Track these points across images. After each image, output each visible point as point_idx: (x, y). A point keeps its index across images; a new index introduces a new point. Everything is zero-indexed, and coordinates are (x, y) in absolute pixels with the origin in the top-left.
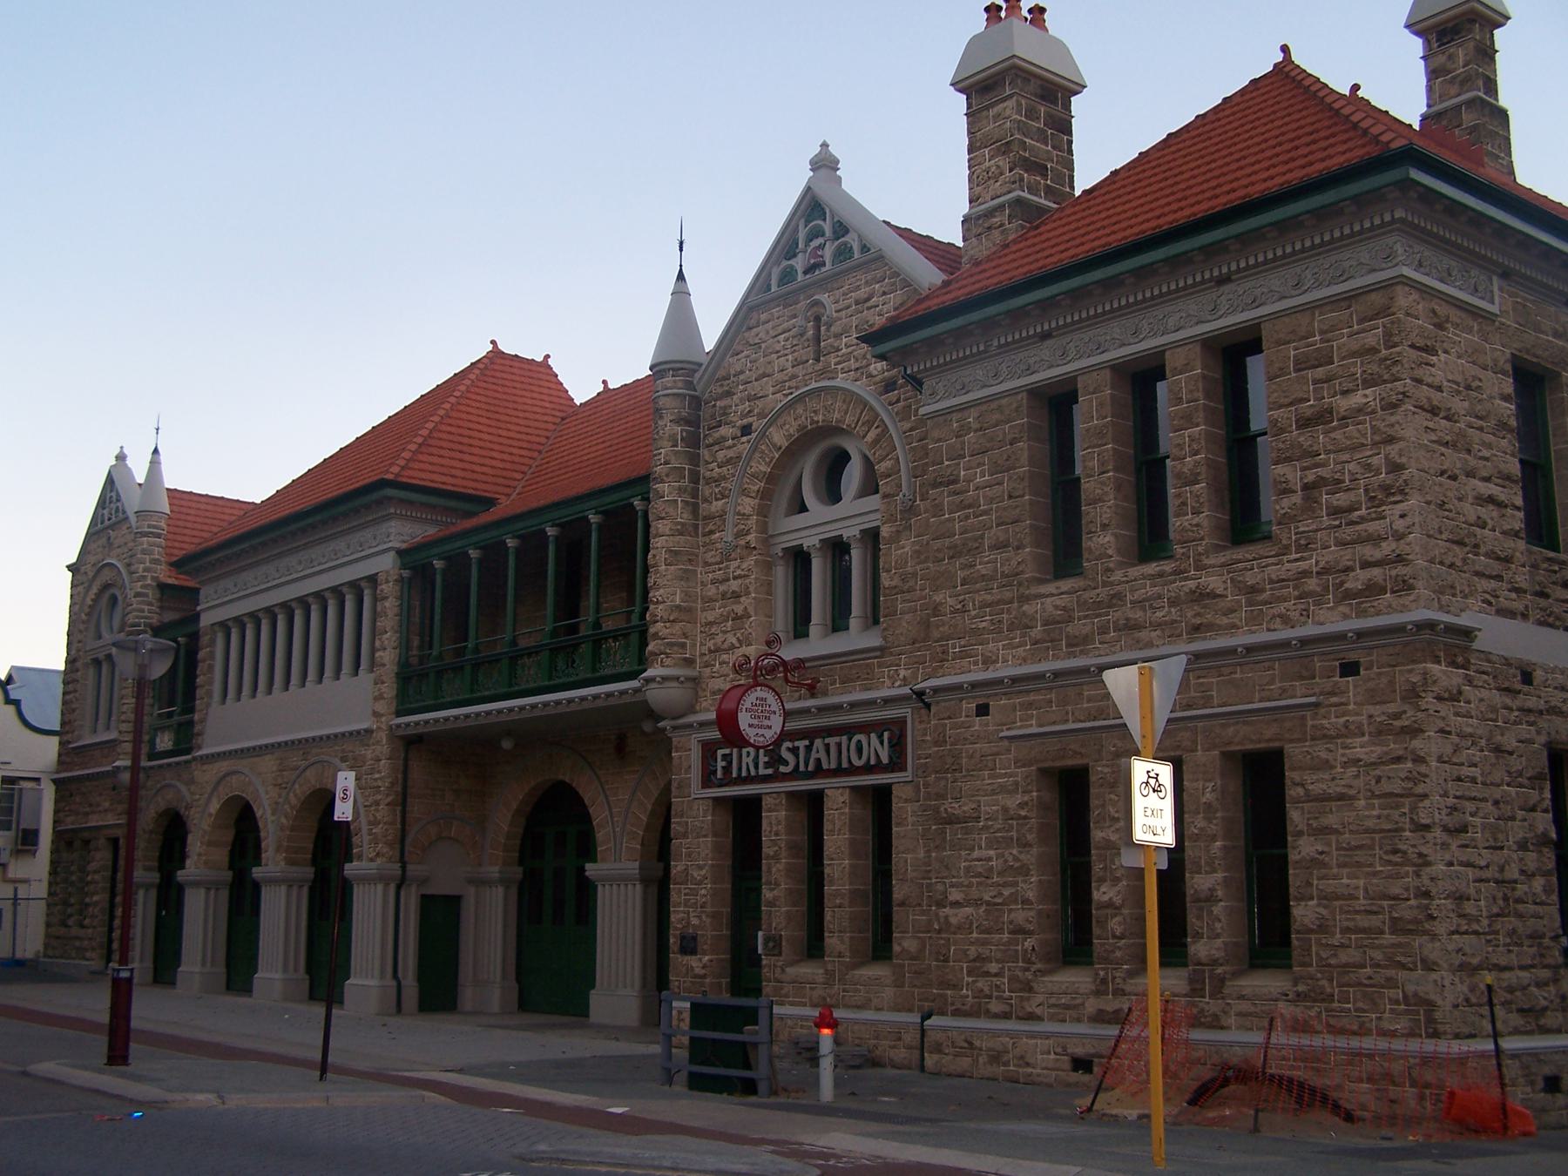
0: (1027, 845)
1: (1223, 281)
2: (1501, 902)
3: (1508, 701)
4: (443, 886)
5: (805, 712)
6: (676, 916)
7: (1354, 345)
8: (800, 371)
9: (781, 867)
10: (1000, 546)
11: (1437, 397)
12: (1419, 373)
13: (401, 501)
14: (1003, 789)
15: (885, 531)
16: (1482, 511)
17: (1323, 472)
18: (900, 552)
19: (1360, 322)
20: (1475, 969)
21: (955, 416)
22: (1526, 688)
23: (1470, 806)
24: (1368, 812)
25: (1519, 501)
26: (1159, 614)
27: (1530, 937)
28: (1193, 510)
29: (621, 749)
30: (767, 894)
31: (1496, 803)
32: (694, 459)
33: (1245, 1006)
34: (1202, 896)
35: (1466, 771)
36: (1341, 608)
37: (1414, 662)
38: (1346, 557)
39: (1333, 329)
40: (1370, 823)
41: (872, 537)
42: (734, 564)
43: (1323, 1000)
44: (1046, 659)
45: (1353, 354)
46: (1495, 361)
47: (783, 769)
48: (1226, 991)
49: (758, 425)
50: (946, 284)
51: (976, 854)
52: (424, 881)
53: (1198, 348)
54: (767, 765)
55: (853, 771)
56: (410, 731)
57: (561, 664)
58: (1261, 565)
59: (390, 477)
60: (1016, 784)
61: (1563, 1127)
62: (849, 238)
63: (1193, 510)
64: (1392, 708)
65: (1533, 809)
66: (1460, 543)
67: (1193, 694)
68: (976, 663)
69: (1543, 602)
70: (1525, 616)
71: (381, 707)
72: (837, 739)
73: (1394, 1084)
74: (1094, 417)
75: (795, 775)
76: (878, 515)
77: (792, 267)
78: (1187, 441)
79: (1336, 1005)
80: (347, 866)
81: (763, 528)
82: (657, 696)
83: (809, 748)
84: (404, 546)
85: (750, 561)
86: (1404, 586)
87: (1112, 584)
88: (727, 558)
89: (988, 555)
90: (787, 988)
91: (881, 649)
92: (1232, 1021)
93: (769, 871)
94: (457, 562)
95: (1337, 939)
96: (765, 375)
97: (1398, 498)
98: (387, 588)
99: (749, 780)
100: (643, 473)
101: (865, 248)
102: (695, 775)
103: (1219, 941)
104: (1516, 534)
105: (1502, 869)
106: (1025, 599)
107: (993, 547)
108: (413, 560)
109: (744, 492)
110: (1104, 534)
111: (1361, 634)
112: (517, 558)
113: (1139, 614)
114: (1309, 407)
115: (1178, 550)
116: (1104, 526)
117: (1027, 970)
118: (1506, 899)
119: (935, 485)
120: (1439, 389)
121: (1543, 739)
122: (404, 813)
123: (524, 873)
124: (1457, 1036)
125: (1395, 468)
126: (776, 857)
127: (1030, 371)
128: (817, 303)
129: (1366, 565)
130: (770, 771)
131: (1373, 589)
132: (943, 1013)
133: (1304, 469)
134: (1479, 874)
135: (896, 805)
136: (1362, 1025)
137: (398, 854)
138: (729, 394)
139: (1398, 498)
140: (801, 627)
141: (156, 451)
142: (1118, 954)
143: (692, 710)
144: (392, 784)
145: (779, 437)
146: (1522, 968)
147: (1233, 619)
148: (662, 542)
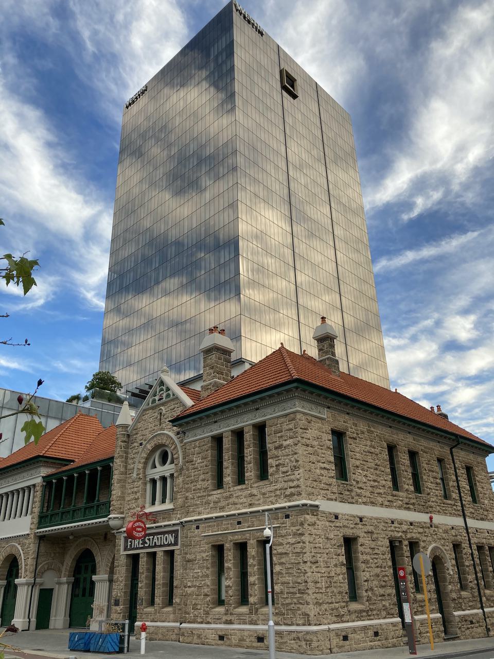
0: (208, 568)
1: (257, 409)
2: (329, 583)
3: (331, 524)
4: (47, 586)
5: (152, 528)
7: (287, 428)
8: (156, 428)
9: (144, 576)
10: (203, 480)
11: (308, 442)
12: (303, 435)
13: (45, 462)
14: (202, 551)
15: (175, 475)
16: (322, 472)
17: (280, 461)
19: (289, 421)
20: (320, 604)
21: (193, 443)
22: (336, 520)
23: (319, 555)
24: (292, 558)
25: (334, 468)
26: (242, 500)
27: (338, 593)
28: (251, 472)
29: (105, 538)
30: (140, 585)
31: (327, 554)
32: (127, 453)
34: (252, 583)
35: (317, 545)
36: (285, 499)
37: (302, 515)
38: (286, 485)
39: (282, 423)
40: (293, 561)
41: (172, 475)
42: (136, 483)
43: (282, 615)
44: (214, 513)
45: (287, 430)
46: (326, 430)
47: (146, 545)
48: (258, 613)
49: (144, 443)
50: (193, 406)
51: (195, 571)
52: (41, 584)
53: (251, 427)
54: (142, 544)
55: (164, 545)
56: (41, 534)
57: (64, 517)
58: (266, 487)
59: (42, 454)
60: (206, 549)
61: (492, 650)
63: (251, 472)
64: (297, 528)
65: (339, 555)
66: (316, 481)
67: (250, 523)
68: (196, 514)
69: (341, 496)
70: (336, 500)
71: (33, 526)
72: (160, 536)
73: (300, 640)
75: (149, 547)
76: (173, 470)
77: (169, 393)
78: (250, 453)
80: (16, 580)
81: (144, 473)
82: (111, 523)
83: (153, 539)
84: (44, 475)
86: (299, 494)
87: (230, 491)
88: (134, 482)
90: (144, 616)
91: (173, 509)
92: (260, 622)
93: (141, 577)
94: (60, 481)
96: (146, 429)
98: (38, 488)
99: (137, 548)
100: (111, 456)
101: (174, 395)
102: (122, 548)
103: (256, 597)
104: (333, 477)
105: (329, 573)
106: (209, 495)
107: (201, 480)
108: (47, 479)
109: (139, 462)
111: (289, 507)
112: (101, 473)
113: (236, 500)
114: (277, 444)
115: (246, 482)
116: (229, 475)
117: (208, 607)
118: (330, 582)
119: (188, 462)
120: (309, 439)
121: (342, 535)
122: (37, 562)
123: (75, 580)
124: (315, 625)
125: (297, 461)
126: (143, 573)
127: (211, 431)
128: (161, 409)
130: (142, 546)
131: (292, 495)
132: (185, 623)
133: (276, 460)
134: (322, 575)
136: (292, 622)
137: (33, 575)
138: (137, 434)
140: (153, 503)
142: (231, 601)
144: (34, 551)
145: (149, 447)
146: (336, 603)
148: (116, 477)
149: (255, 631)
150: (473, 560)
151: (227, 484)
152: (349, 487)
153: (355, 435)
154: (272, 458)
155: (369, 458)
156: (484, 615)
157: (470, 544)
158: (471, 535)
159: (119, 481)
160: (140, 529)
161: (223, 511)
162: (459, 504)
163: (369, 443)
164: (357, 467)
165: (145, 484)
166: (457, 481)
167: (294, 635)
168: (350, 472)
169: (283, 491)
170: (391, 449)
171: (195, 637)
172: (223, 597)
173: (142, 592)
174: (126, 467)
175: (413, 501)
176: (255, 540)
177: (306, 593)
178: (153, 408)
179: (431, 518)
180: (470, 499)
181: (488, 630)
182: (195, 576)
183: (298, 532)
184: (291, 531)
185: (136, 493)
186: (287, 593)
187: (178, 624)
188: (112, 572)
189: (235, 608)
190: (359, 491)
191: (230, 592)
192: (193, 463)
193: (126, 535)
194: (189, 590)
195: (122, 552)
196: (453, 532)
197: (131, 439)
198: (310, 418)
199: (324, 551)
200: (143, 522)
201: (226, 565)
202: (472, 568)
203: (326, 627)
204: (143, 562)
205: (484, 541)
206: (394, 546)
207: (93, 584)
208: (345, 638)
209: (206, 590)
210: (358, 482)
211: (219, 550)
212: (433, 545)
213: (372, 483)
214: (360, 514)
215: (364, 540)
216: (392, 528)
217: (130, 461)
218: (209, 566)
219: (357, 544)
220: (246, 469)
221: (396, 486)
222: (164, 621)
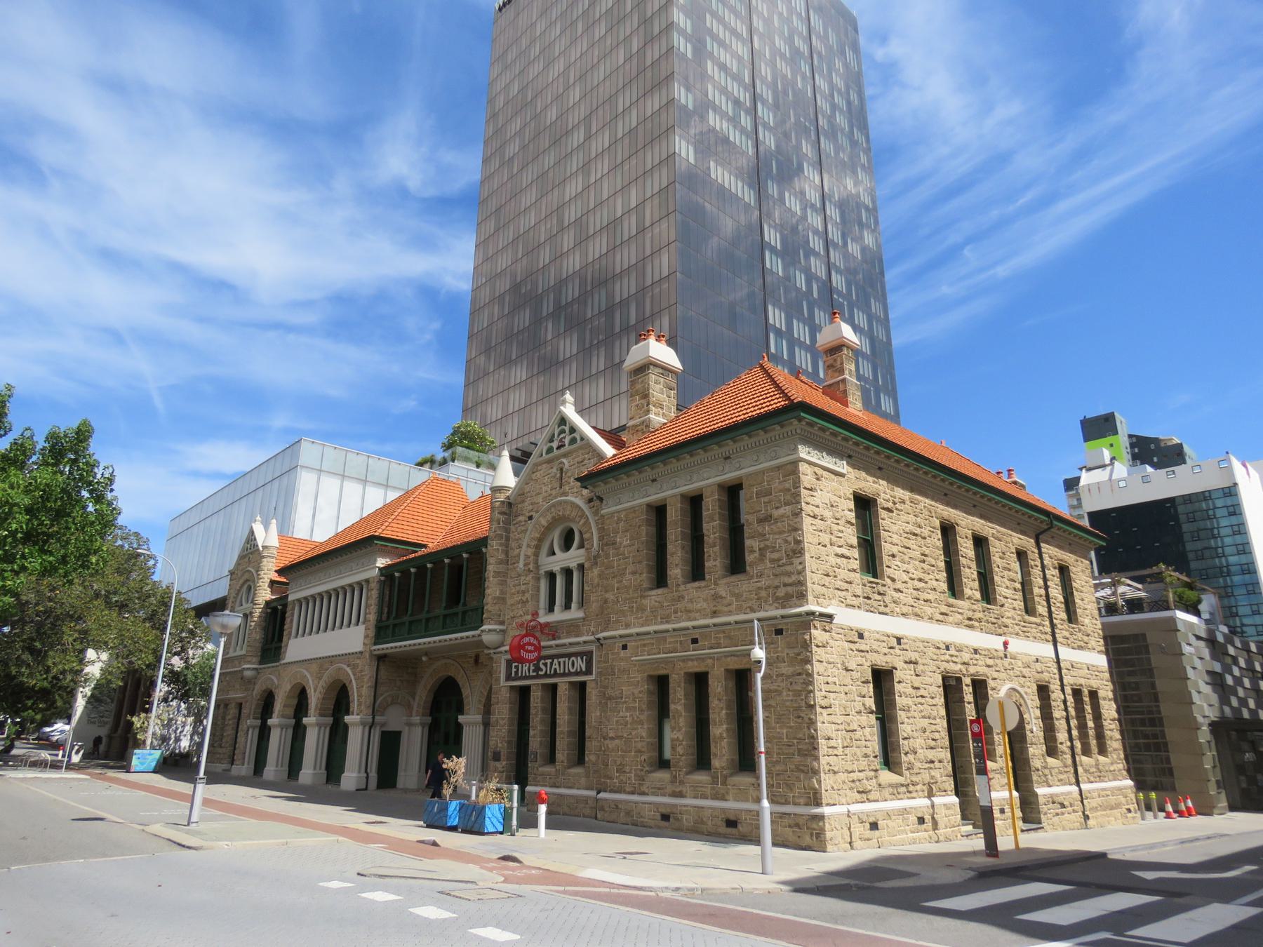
4: (392, 727)
6: (492, 743)
7: (781, 487)
8: (554, 492)
11: (817, 511)
18: (593, 574)
25: (857, 556)
28: (715, 559)
29: (477, 660)
30: (532, 732)
32: (507, 531)
38: (776, 582)
41: (581, 567)
49: (536, 516)
52: (383, 725)
55: (570, 674)
58: (743, 584)
63: (715, 559)
64: (796, 651)
66: (827, 575)
74: (712, 509)
75: (546, 676)
78: (713, 529)
82: (486, 638)
85: (530, 577)
89: (628, 576)
90: (539, 778)
94: (405, 573)
101: (582, 439)
102: (503, 676)
104: (854, 571)
110: (677, 567)
115: (707, 577)
119: (607, 545)
129: (785, 585)
131: (788, 597)
135: (588, 690)
140: (551, 609)
143: (502, 645)
145: (544, 522)
147: (730, 608)
148: (491, 568)
149: (723, 810)
150: (1066, 710)
152: (881, 589)
153: (890, 505)
155: (912, 543)
156: (1081, 795)
157: (1062, 686)
158: (1064, 671)
159: (497, 574)
160: (531, 648)
161: (668, 622)
162: (1047, 623)
163: (911, 518)
164: (893, 556)
165: (538, 579)
166: (1046, 587)
170: (948, 530)
172: (667, 754)
173: (536, 740)
174: (507, 553)
175: (978, 615)
178: (549, 461)
179: (1006, 644)
180: (1064, 616)
181: (1086, 818)
185: (524, 592)
187: (593, 793)
188: (487, 711)
189: (688, 773)
191: (680, 750)
193: (509, 657)
194: (612, 744)
195: (503, 683)
196: (1038, 666)
197: (514, 509)
198: (820, 472)
199: (842, 689)
200: (535, 637)
201: (672, 707)
202: (1063, 722)
203: (843, 809)
204: (536, 699)
205: (1082, 681)
206: (951, 686)
207: (459, 727)
208: (874, 826)
209: (639, 745)
210: (893, 580)
211: (662, 683)
212: (1008, 686)
213: (916, 583)
214: (899, 633)
216: (947, 657)
217: (513, 544)
218: (644, 707)
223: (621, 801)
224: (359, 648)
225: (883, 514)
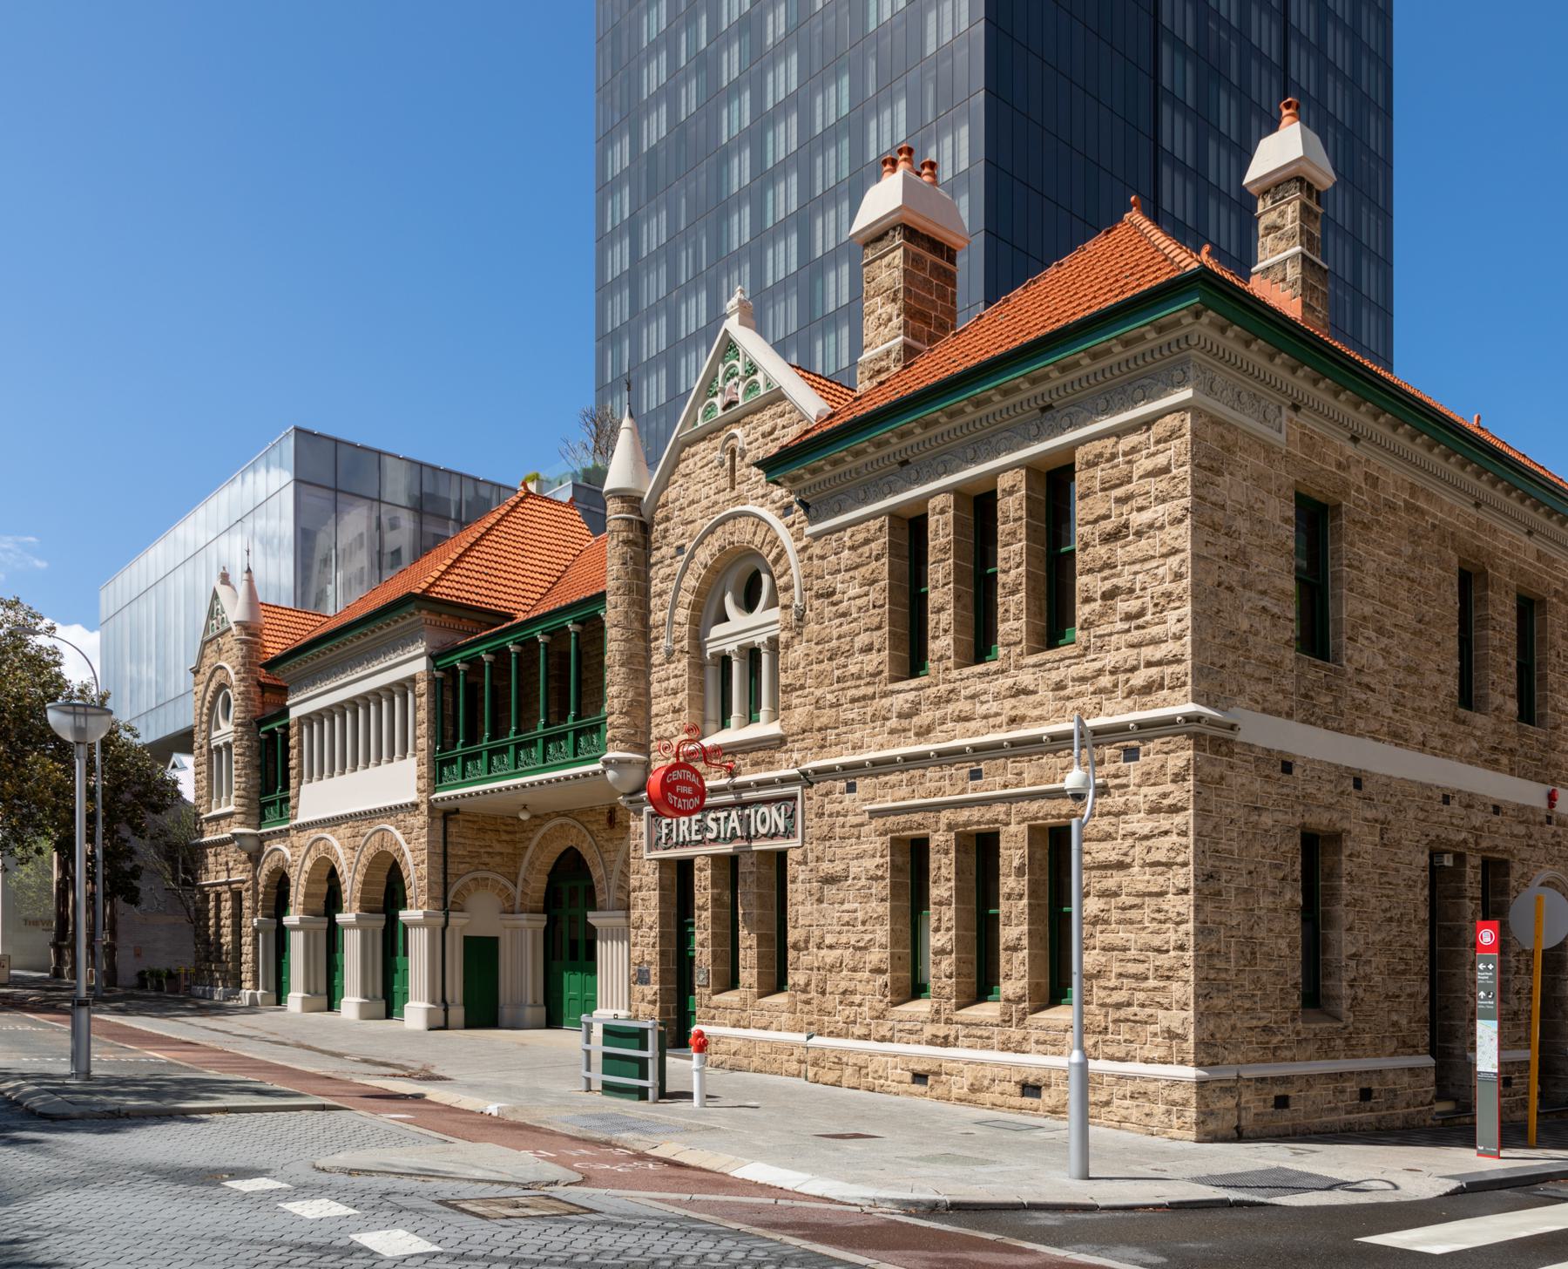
4: (482, 929)
8: (721, 497)
17: (1121, 582)
25: (1292, 615)
26: (985, 707)
33: (1041, 1035)
41: (773, 642)
48: (1027, 1022)
49: (689, 546)
51: (846, 906)
58: (1063, 664)
60: (875, 849)
62: (759, 377)
64: (1160, 789)
70: (1289, 715)
78: (1013, 559)
79: (1109, 1036)
95: (1113, 983)
96: (692, 502)
97: (1177, 604)
99: (684, 844)
107: (862, 651)
111: (1141, 725)
115: (1001, 651)
116: (946, 631)
128: (734, 437)
129: (1149, 664)
130: (699, 837)
131: (1147, 689)
139: (1177, 604)
141: (249, 571)
151: (940, 659)
154: (1090, 571)
160: (689, 790)
167: (1129, 1088)
168: (1339, 634)
169: (1122, 677)
171: (849, 1071)
173: (703, 955)
176: (1025, 825)
177: (1179, 979)
179: (1552, 797)
182: (843, 917)
183: (1166, 802)
184: (1141, 799)
186: (1120, 975)
187: (802, 1037)
190: (1361, 696)
192: (835, 598)
211: (912, 858)
215: (1361, 844)
219: (1338, 852)
220: (1001, 610)
221: (1468, 697)
222: (765, 1028)
223: (849, 1051)
224: (413, 797)
225: (1352, 532)
